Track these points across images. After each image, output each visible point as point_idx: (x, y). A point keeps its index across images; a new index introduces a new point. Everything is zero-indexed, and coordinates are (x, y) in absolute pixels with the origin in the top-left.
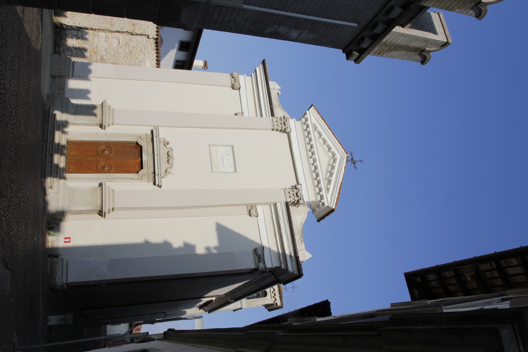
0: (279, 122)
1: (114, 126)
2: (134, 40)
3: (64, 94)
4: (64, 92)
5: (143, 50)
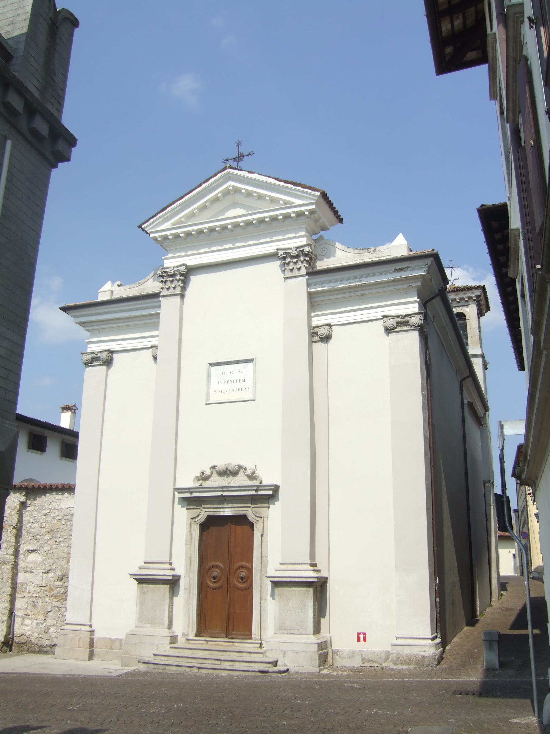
0: (168, 285)
1: (173, 561)
2: (28, 525)
3: (121, 640)
4: (116, 639)
5: (45, 512)
